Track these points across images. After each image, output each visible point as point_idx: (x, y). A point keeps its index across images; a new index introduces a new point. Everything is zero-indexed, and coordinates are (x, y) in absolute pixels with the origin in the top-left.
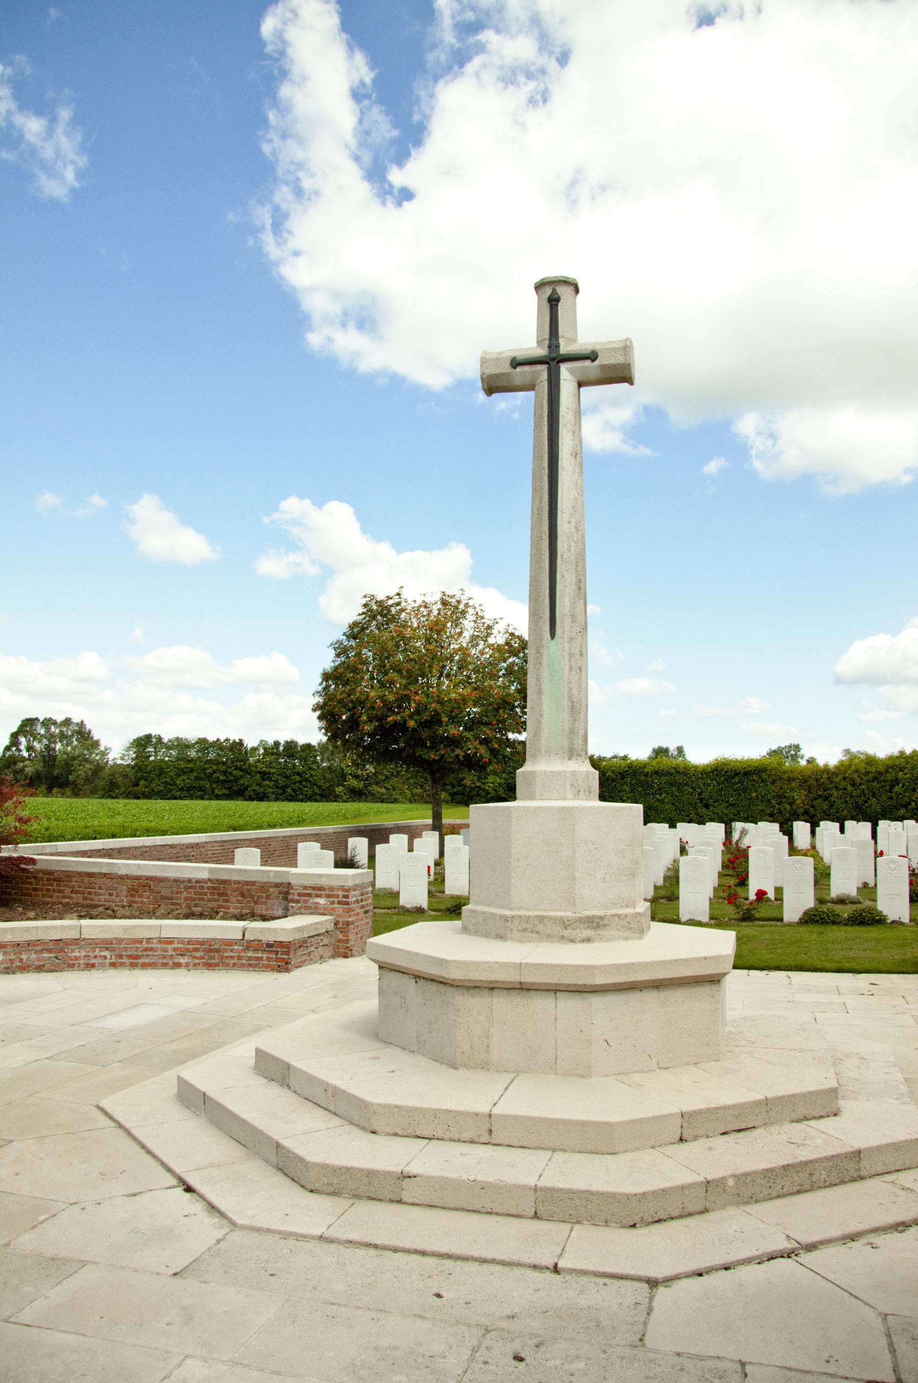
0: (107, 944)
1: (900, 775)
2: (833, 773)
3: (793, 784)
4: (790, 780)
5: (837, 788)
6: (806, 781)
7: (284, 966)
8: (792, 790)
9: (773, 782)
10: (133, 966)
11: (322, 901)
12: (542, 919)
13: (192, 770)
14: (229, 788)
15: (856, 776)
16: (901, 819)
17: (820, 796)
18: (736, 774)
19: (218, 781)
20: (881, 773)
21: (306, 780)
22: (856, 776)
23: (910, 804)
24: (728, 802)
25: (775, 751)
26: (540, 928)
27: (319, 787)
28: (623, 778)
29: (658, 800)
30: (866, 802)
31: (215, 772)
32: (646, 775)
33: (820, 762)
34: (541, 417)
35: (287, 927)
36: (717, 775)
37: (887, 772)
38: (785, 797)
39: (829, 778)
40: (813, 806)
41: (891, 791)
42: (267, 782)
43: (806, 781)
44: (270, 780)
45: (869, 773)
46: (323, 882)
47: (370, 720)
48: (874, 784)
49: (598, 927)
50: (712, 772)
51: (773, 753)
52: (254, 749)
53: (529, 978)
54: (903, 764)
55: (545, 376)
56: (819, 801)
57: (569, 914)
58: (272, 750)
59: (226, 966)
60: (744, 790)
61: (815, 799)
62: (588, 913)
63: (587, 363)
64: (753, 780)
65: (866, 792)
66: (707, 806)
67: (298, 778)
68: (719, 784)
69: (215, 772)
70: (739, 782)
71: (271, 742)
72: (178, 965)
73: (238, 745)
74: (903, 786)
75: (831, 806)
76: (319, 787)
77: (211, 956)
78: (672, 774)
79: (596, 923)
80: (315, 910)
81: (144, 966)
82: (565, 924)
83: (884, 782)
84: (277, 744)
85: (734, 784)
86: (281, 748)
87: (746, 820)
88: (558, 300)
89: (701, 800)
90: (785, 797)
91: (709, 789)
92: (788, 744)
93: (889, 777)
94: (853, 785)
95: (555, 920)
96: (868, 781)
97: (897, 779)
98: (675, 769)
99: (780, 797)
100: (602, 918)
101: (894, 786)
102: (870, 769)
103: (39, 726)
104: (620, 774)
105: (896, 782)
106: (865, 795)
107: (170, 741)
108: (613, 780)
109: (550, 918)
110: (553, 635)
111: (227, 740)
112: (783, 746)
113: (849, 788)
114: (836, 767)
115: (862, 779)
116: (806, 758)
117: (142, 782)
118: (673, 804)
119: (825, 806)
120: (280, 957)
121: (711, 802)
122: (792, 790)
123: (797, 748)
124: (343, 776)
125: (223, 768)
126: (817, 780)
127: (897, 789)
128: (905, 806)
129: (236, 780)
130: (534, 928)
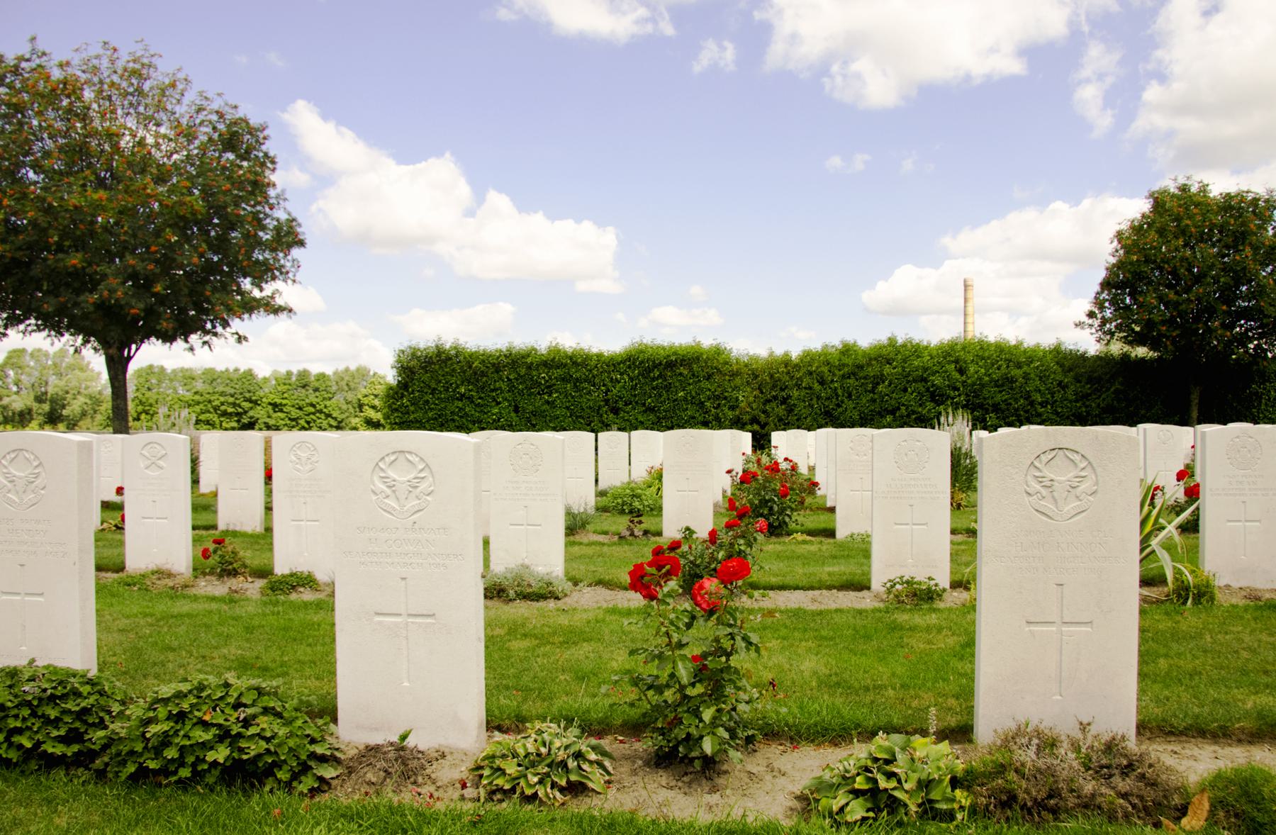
1: (887, 369)
2: (796, 365)
4: (734, 374)
5: (799, 386)
6: (757, 377)
8: (736, 388)
9: (709, 377)
13: (198, 403)
14: (238, 421)
15: (825, 369)
18: (656, 366)
19: (225, 414)
20: (861, 367)
21: (321, 412)
22: (825, 369)
23: (899, 409)
24: (644, 405)
27: (335, 419)
28: (497, 372)
29: (548, 402)
30: (839, 406)
31: (222, 404)
32: (529, 367)
36: (629, 367)
37: (869, 364)
38: (725, 398)
39: (788, 373)
40: (764, 412)
41: (872, 391)
42: (279, 414)
43: (757, 377)
44: (281, 411)
45: (844, 365)
48: (851, 381)
50: (623, 362)
52: (266, 380)
54: (892, 355)
56: (774, 404)
58: (285, 381)
60: (668, 388)
61: (769, 401)
64: (681, 374)
65: (840, 392)
66: (615, 411)
67: (312, 410)
68: (631, 379)
69: (222, 404)
70: (660, 376)
71: (283, 370)
73: (249, 374)
74: (890, 385)
75: (790, 411)
76: (335, 419)
78: (565, 365)
83: (865, 378)
84: (289, 374)
85: (654, 379)
86: (294, 379)
89: (607, 401)
90: (725, 398)
91: (618, 386)
93: (871, 371)
94: (822, 383)
96: (843, 376)
97: (882, 375)
98: (571, 358)
99: (718, 398)
101: (878, 384)
102: (846, 360)
103: (28, 358)
104: (494, 365)
105: (879, 379)
106: (837, 395)
107: (174, 371)
108: (483, 374)
111: (236, 370)
113: (816, 386)
115: (834, 375)
117: (143, 416)
118: (568, 408)
119: (781, 410)
121: (621, 404)
122: (736, 388)
124: (361, 406)
125: (231, 400)
126: (772, 376)
127: (880, 388)
128: (893, 412)
129: (246, 412)
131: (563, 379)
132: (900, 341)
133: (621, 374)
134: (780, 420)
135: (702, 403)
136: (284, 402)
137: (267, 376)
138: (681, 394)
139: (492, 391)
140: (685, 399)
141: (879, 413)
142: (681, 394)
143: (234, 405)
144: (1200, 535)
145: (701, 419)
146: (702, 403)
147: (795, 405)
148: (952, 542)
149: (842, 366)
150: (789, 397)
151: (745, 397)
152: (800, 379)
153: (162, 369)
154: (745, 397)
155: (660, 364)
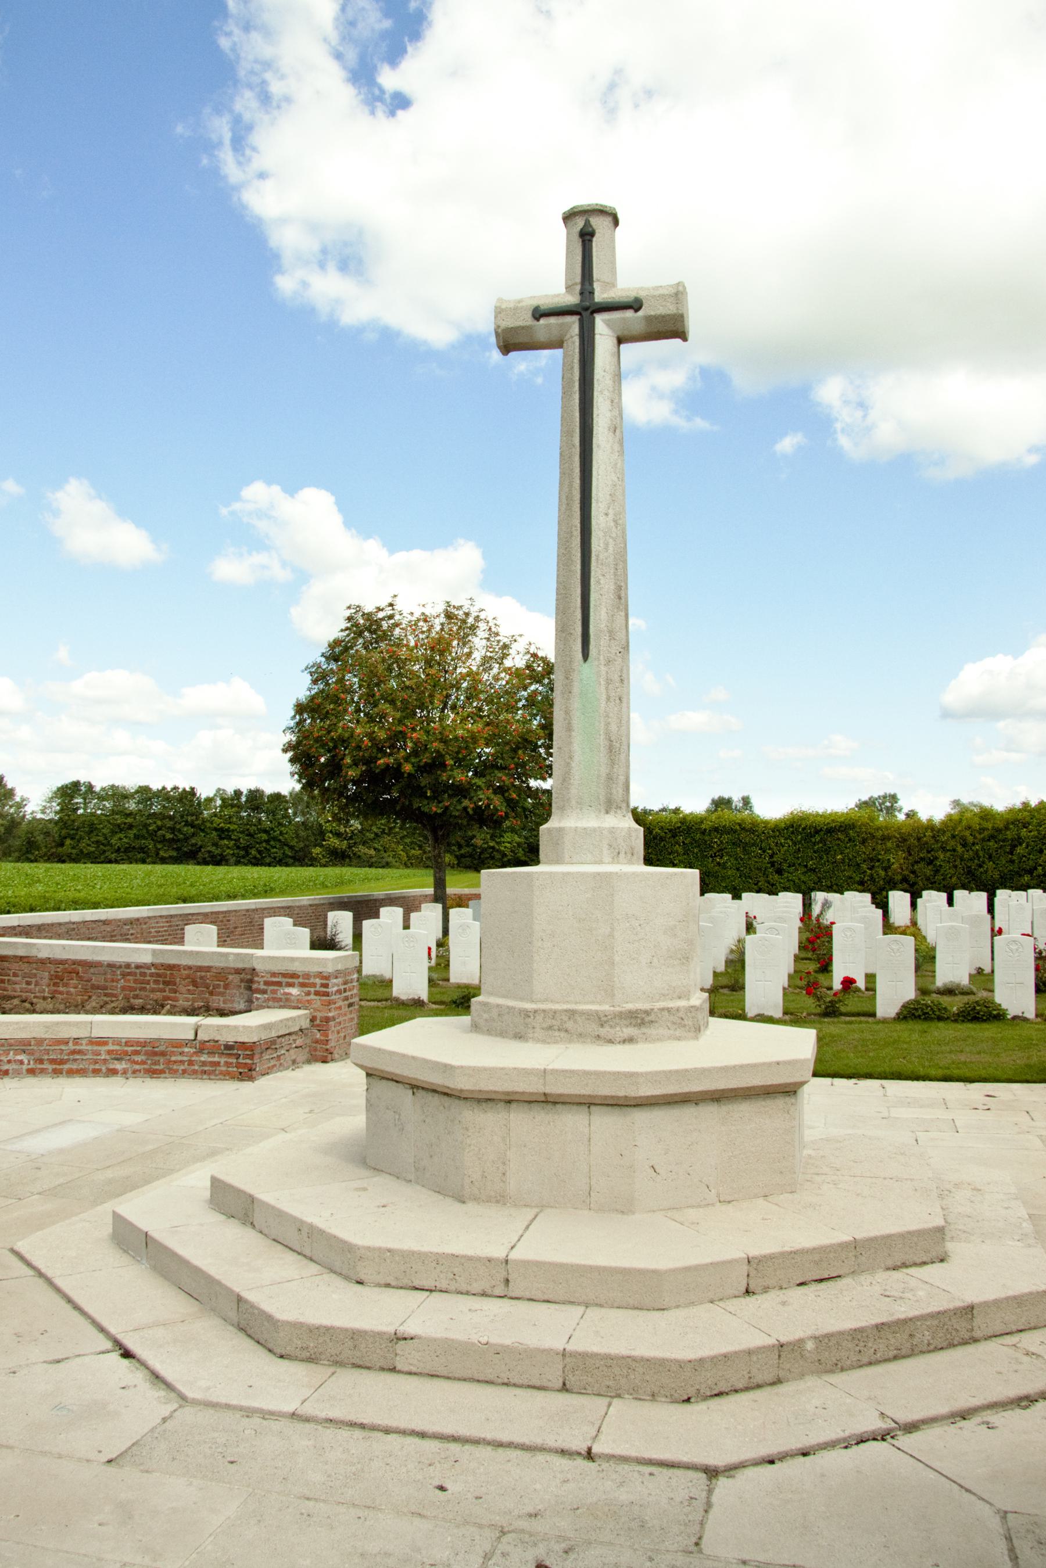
2: (939, 830)
3: (889, 844)
4: (885, 838)
7: (247, 1074)
10: (57, 1073)
11: (294, 991)
12: (572, 1013)
13: (131, 827)
14: (178, 849)
15: (967, 833)
16: (1025, 888)
17: (922, 859)
18: (817, 832)
19: (164, 840)
20: (999, 830)
21: (275, 839)
22: (967, 833)
23: (1035, 868)
24: (806, 866)
25: (865, 803)
26: (570, 1025)
27: (291, 848)
28: (674, 837)
29: (719, 864)
30: (980, 866)
31: (159, 828)
32: (703, 832)
34: (572, 380)
35: (251, 1024)
36: (793, 833)
37: (1007, 828)
38: (879, 860)
40: (913, 872)
41: (1011, 853)
43: (905, 840)
44: (229, 838)
45: (984, 829)
47: (355, 764)
48: (991, 844)
49: (642, 1023)
52: (209, 800)
54: (1028, 819)
55: (575, 329)
56: (922, 865)
57: (606, 1007)
60: (827, 852)
61: (917, 862)
62: (630, 1006)
63: (629, 314)
64: (838, 839)
65: (981, 854)
66: (779, 872)
67: (265, 836)
68: (795, 844)
69: (159, 828)
70: (820, 841)
71: (230, 791)
72: (113, 1072)
76: (291, 848)
77: (155, 1060)
78: (735, 831)
79: (640, 1019)
80: (286, 1003)
82: (602, 1019)
83: (1003, 841)
84: (238, 793)
85: (814, 844)
86: (244, 799)
87: (829, 889)
88: (592, 234)
89: (773, 864)
90: (879, 860)
91: (783, 850)
92: (882, 794)
94: (964, 845)
95: (589, 1015)
96: (983, 840)
98: (740, 825)
99: (872, 860)
100: (647, 1013)
102: (985, 825)
104: (670, 831)
105: (1018, 841)
106: (979, 857)
108: (662, 839)
109: (582, 1013)
110: (586, 655)
111: (175, 788)
112: (876, 796)
113: (959, 849)
114: (943, 823)
115: (975, 838)
116: (905, 810)
118: (738, 869)
119: (928, 871)
120: (242, 1062)
121: (785, 866)
122: (887, 851)
123: (894, 798)
126: (919, 839)
128: (1030, 872)
129: (186, 839)
130: (562, 1026)
131: (734, 844)
132: (1033, 803)
133: (786, 839)
134: (928, 879)
135: (858, 865)
136: (232, 827)
137: (211, 795)
138: (839, 857)
139: (670, 854)
140: (843, 861)
141: (1017, 873)
142: (839, 857)
143: (172, 830)
144: (642, 294)
145: (857, 879)
146: (858, 865)
147: (941, 866)
148: (992, 991)
149: (982, 830)
150: (936, 858)
151: (897, 860)
152: (946, 842)
153: (90, 787)
154: (897, 860)
155: (821, 830)
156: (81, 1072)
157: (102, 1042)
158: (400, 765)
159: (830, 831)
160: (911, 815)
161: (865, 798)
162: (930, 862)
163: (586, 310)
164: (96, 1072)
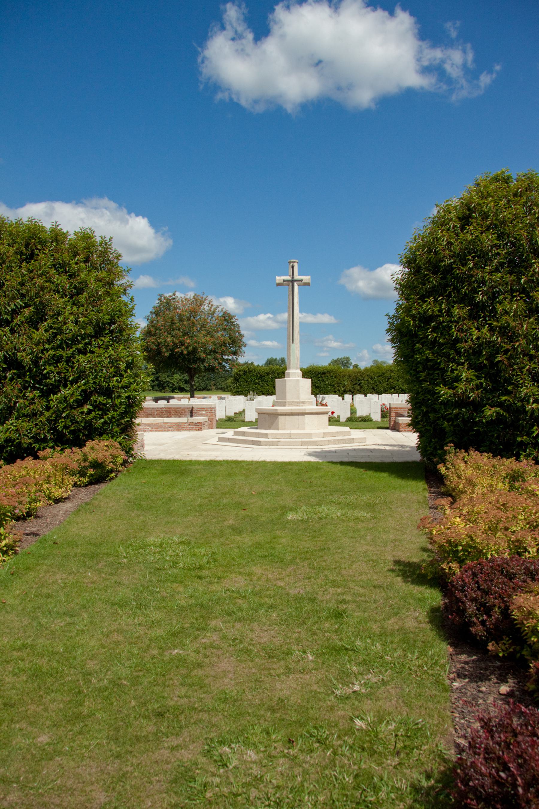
0: (149, 425)
4: (344, 376)
7: (200, 429)
10: (156, 431)
11: (204, 412)
16: (392, 393)
20: (384, 373)
25: (336, 361)
33: (256, 364)
35: (197, 419)
46: (204, 407)
47: (167, 351)
51: (335, 362)
53: (293, 411)
59: (183, 430)
72: (169, 430)
77: (179, 427)
79: (304, 403)
80: (202, 415)
81: (159, 431)
82: (298, 403)
87: (324, 394)
94: (371, 379)
114: (364, 370)
116: (353, 364)
119: (358, 387)
120: (199, 426)
123: (348, 359)
128: (394, 388)
130: (291, 404)
156: (162, 431)
157: (166, 423)
158: (182, 351)
159: (324, 373)
160: (356, 366)
161: (335, 359)
162: (359, 385)
163: (293, 281)
164: (165, 431)
